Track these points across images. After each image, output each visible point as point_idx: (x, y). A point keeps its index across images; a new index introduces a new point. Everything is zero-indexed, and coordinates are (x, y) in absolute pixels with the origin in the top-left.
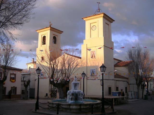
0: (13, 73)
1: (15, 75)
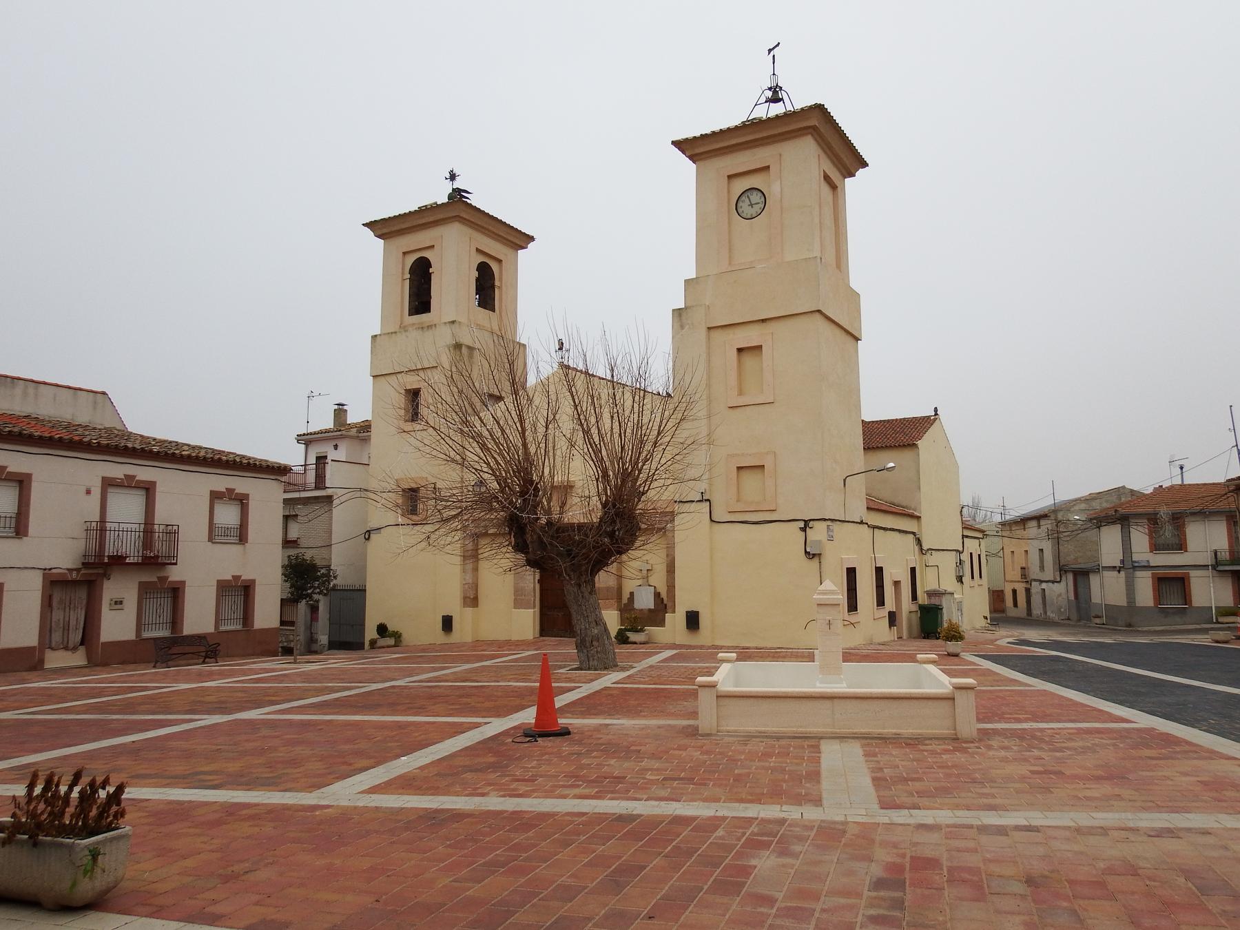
0: (230, 491)
1: (242, 501)
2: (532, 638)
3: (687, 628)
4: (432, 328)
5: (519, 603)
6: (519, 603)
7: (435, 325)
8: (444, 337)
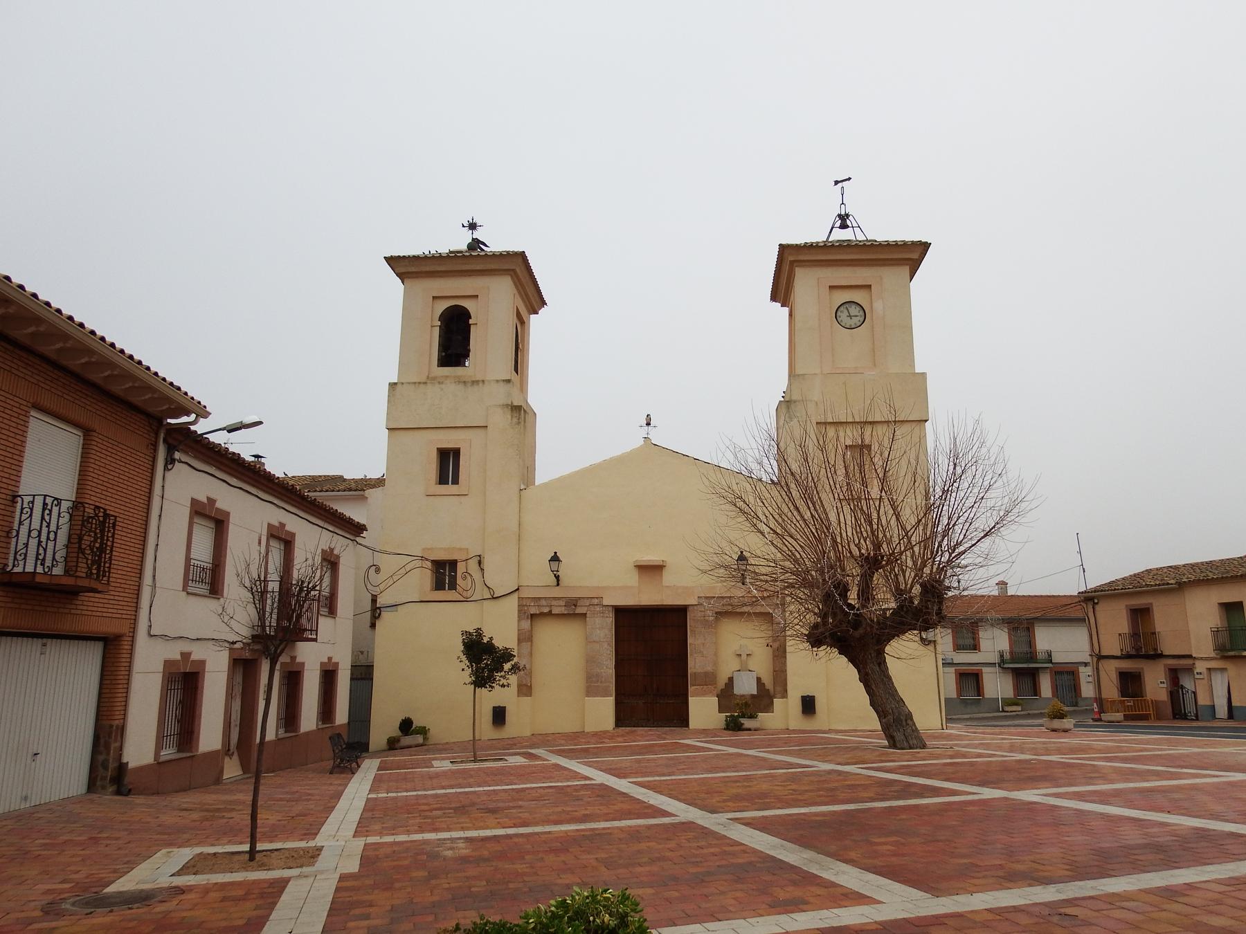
3: (493, 723)
4: (478, 384)
5: (592, 689)
6: (592, 689)
7: (483, 381)
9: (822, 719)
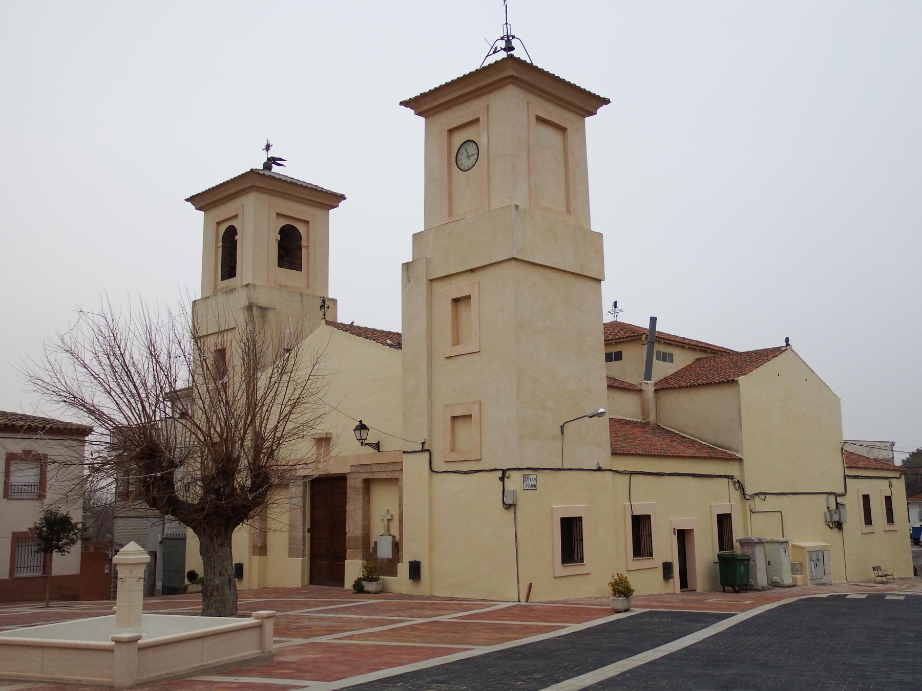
0: (27, 453)
2: (300, 586)
5: (292, 553)
6: (292, 553)
8: (241, 299)
9: (424, 588)
